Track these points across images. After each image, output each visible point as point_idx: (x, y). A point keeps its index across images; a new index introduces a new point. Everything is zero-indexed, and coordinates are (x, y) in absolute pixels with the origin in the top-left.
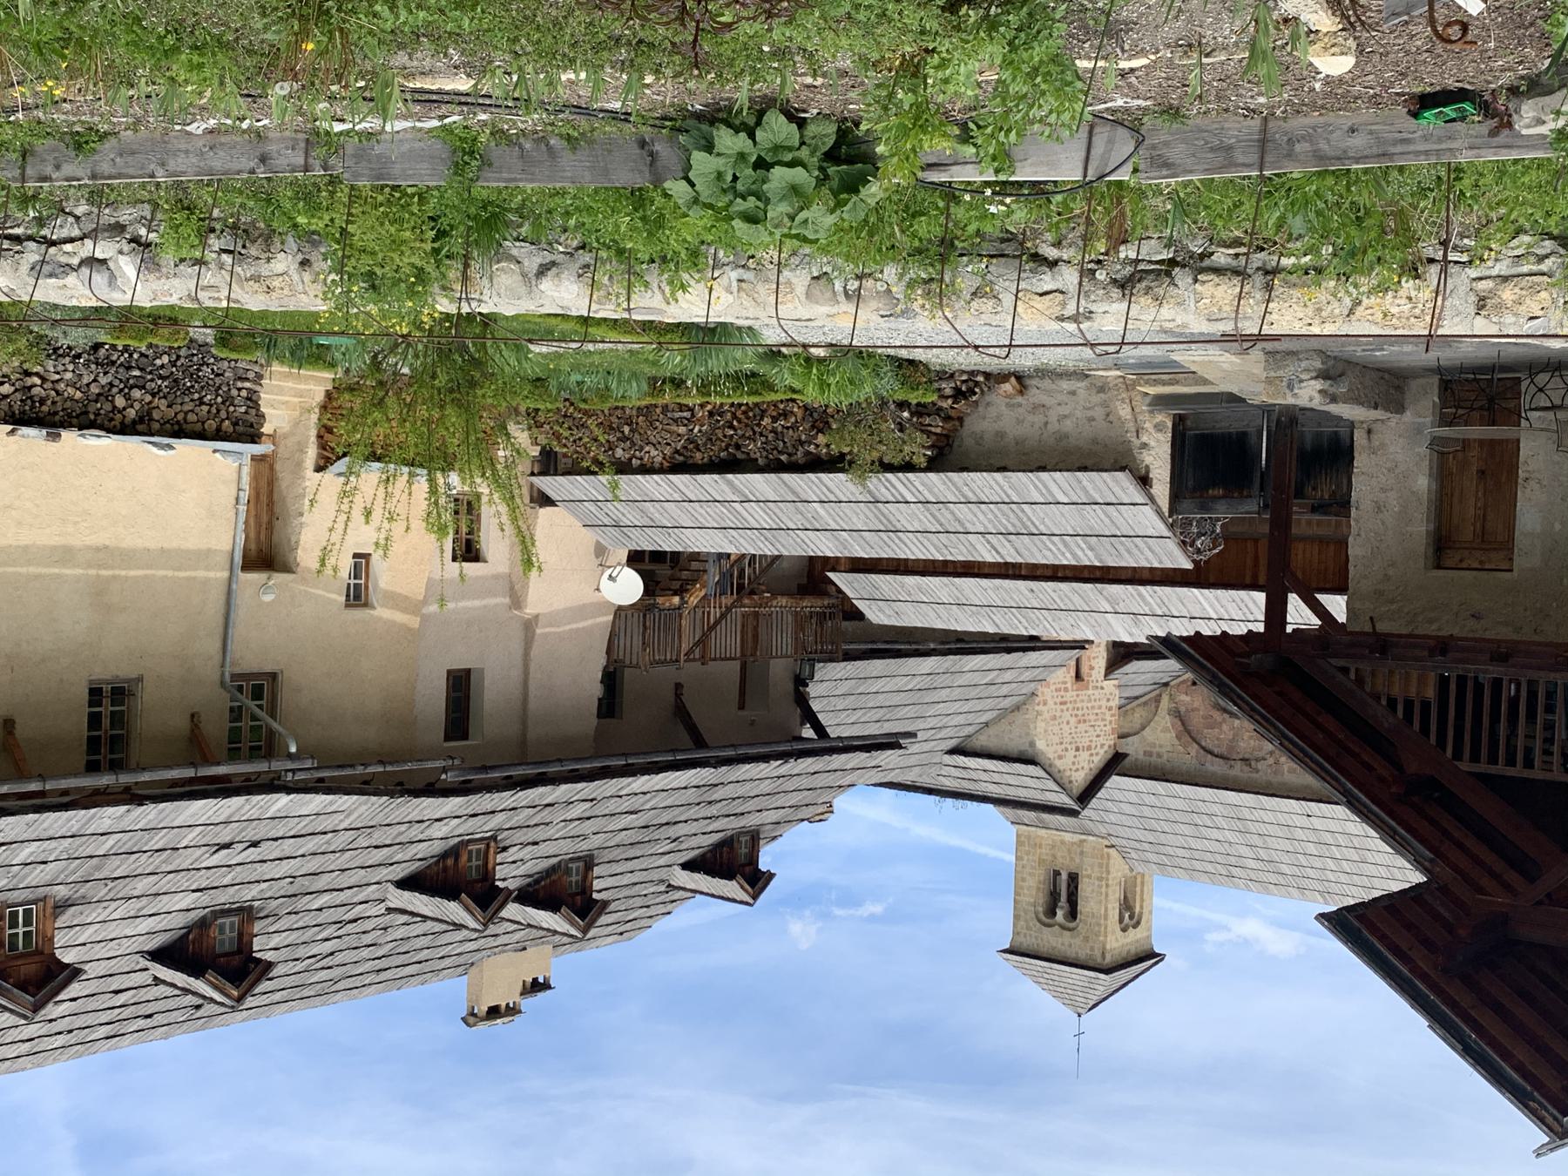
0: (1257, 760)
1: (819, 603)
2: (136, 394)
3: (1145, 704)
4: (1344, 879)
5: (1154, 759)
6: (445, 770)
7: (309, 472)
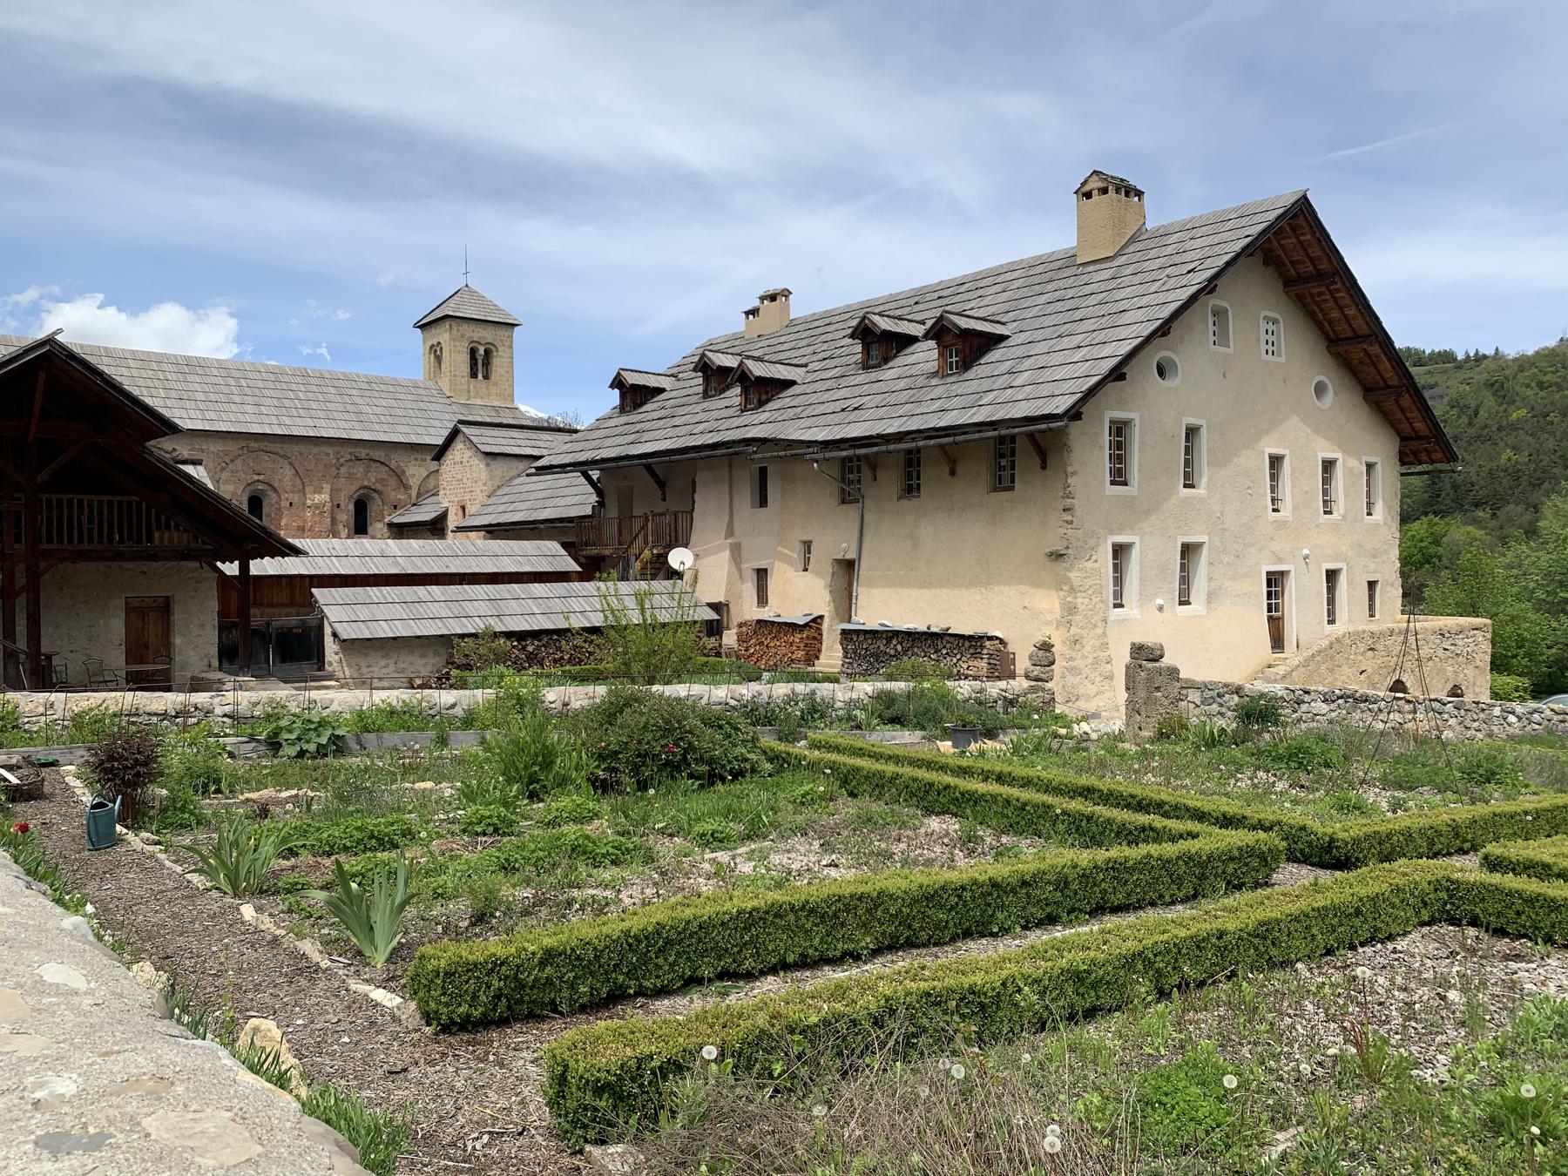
0: (351, 460)
1: (588, 552)
2: (892, 652)
3: (427, 492)
4: (294, 387)
5: (419, 457)
6: (755, 452)
7: (826, 615)
